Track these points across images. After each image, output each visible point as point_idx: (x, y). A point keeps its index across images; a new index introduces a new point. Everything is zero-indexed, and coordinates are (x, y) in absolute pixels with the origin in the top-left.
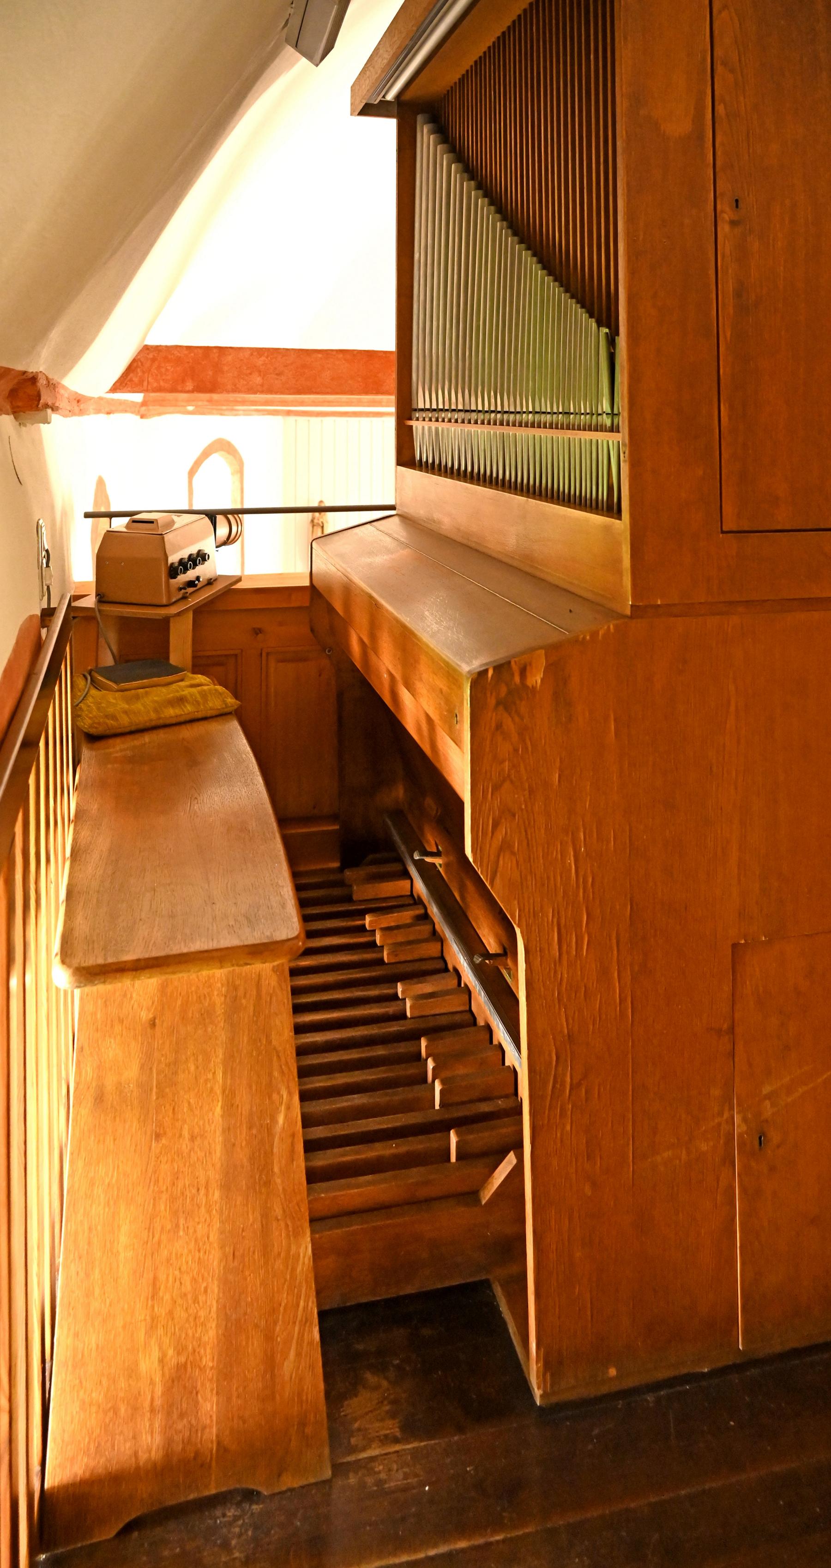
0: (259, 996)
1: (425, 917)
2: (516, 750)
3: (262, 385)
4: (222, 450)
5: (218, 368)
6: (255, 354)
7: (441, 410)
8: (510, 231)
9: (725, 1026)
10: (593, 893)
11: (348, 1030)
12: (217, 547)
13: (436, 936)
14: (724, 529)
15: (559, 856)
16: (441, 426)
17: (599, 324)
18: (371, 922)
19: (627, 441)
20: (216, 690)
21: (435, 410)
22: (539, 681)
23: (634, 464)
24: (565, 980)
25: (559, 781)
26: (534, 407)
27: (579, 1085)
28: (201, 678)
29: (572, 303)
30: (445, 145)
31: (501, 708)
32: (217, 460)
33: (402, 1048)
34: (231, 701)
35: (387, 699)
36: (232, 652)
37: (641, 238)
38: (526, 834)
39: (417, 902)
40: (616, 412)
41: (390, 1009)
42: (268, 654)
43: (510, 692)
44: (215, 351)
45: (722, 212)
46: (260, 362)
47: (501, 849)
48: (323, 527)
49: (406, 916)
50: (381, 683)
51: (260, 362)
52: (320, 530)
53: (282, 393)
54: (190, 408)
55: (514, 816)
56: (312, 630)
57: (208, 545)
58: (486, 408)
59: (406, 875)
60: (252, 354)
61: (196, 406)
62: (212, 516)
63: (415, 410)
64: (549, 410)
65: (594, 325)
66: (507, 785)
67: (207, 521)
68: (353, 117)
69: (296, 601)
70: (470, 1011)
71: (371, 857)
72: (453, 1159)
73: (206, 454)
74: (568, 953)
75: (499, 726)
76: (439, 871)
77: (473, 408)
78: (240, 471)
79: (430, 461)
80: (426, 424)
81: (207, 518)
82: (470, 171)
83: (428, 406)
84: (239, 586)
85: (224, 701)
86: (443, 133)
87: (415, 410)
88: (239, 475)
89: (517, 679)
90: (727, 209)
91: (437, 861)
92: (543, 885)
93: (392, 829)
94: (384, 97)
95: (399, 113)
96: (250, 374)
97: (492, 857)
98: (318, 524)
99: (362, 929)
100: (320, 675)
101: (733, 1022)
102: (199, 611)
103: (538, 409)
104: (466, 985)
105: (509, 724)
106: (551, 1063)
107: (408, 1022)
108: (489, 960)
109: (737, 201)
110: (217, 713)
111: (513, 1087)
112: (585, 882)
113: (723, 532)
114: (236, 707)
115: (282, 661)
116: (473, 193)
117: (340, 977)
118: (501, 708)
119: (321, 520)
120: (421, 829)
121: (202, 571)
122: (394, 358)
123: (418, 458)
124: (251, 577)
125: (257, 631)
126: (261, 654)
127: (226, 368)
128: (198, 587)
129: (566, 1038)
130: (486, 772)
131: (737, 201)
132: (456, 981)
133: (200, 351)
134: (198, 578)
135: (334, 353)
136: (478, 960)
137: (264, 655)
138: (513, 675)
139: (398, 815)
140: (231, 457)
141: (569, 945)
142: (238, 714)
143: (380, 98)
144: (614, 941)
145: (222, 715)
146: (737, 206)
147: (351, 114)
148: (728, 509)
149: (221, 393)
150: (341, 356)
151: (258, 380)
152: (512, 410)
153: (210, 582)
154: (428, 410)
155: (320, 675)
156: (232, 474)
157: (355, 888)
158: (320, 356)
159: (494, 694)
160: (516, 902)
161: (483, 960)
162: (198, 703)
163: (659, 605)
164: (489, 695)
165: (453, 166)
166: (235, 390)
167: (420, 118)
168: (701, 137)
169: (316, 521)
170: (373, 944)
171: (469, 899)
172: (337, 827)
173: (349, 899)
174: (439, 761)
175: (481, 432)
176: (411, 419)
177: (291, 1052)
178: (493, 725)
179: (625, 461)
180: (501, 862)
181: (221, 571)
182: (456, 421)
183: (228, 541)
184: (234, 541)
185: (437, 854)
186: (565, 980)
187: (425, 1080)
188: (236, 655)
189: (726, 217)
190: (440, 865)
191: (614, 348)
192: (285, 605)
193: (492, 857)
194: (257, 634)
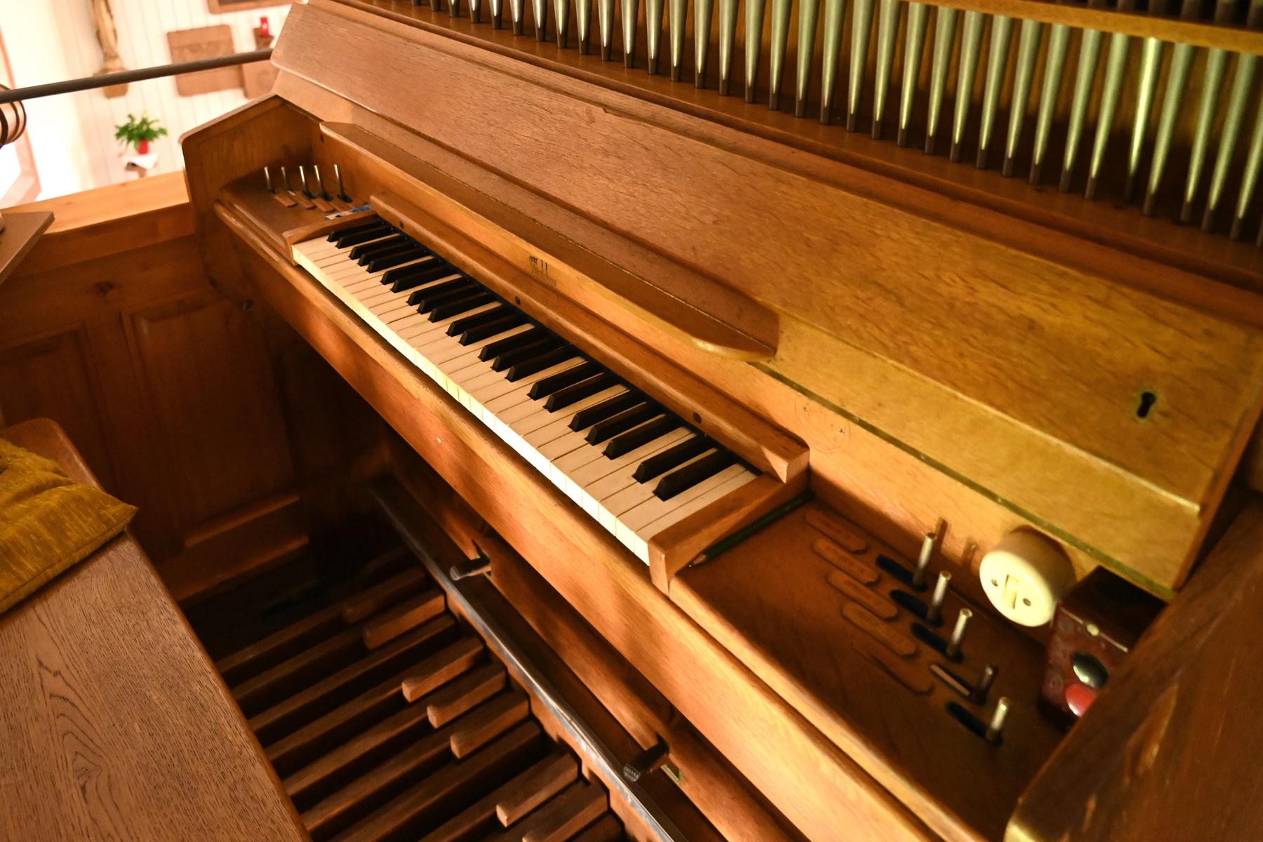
1: (486, 659)
34: (119, 511)
39: (462, 629)
69: (165, 233)
85: (100, 517)
91: (485, 570)
104: (591, 773)
136: (635, 777)
157: (368, 634)
162: (48, 547)
173: (359, 651)
185: (483, 562)
190: (489, 573)
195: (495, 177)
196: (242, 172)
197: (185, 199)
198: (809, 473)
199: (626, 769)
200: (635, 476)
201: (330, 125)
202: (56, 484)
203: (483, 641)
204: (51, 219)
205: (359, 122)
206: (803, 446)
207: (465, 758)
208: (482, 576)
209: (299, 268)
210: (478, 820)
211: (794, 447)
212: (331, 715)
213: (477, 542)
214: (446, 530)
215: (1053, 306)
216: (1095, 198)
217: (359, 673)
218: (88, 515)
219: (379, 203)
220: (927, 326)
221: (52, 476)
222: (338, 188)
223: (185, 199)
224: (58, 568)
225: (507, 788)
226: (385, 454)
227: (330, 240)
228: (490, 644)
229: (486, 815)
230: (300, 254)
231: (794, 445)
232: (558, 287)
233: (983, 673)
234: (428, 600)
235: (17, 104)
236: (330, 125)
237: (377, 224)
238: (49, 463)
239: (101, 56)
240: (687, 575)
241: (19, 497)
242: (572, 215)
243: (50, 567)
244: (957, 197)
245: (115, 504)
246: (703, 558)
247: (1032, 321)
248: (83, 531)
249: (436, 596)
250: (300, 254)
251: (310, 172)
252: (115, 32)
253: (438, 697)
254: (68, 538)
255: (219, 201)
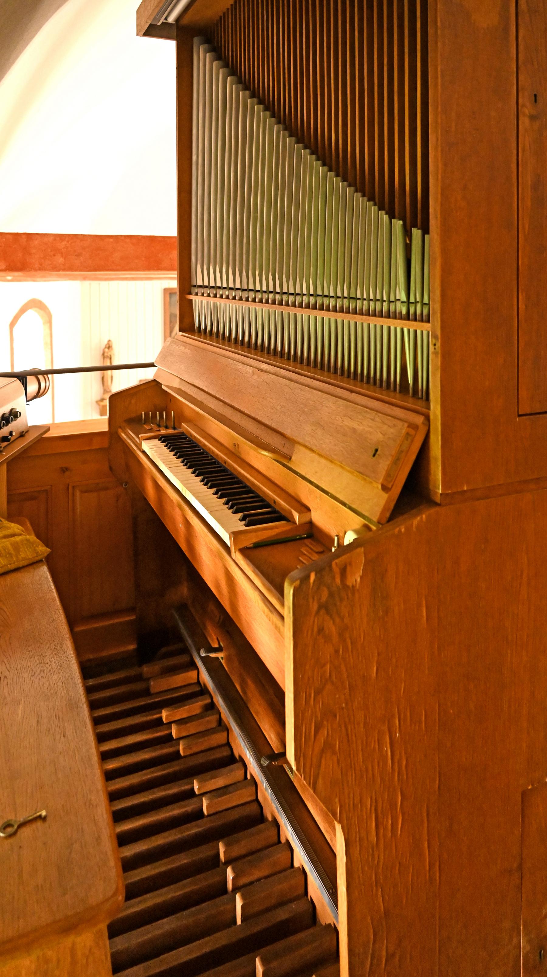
0: (74, 962)
1: (211, 707)
2: (337, 651)
3: (64, 265)
4: (35, 307)
5: (26, 250)
6: (58, 239)
7: (219, 288)
8: (287, 133)
9: (515, 865)
10: (407, 774)
11: (153, 838)
12: (27, 401)
13: (222, 726)
14: (520, 413)
15: (377, 747)
16: (218, 301)
17: (392, 216)
18: (167, 717)
19: (439, 333)
20: (28, 540)
21: (213, 287)
22: (359, 580)
23: (446, 356)
24: (382, 861)
25: (377, 673)
26: (315, 290)
27: (393, 955)
28: (15, 527)
29: (358, 195)
30: (220, 62)
31: (323, 611)
32: (32, 314)
33: (202, 853)
34: (43, 550)
35: (183, 546)
36: (43, 488)
37: (453, 128)
38: (347, 730)
39: (204, 691)
40: (412, 300)
41: (188, 807)
42: (73, 487)
43: (331, 595)
44: (23, 236)
45: (524, 106)
46: (62, 245)
47: (323, 751)
48: (111, 359)
49: (195, 707)
50: (177, 530)
51: (62, 245)
52: (108, 361)
53: (81, 271)
54: (9, 278)
55: (336, 716)
56: (111, 468)
57: (19, 403)
58: (264, 289)
59: (193, 665)
60: (55, 240)
61: (14, 276)
62: (22, 377)
63: (195, 286)
64: (332, 294)
65: (386, 218)
66: (329, 686)
67: (18, 383)
68: (139, 37)
69: (96, 444)
70: (257, 800)
71: (164, 650)
72: (239, 922)
73: (23, 310)
74: (385, 835)
75: (321, 630)
76: (220, 662)
77: (251, 287)
78: (49, 321)
79: (209, 328)
80: (205, 300)
81: (18, 381)
82: (244, 83)
83: (206, 283)
84: (47, 435)
85: (35, 550)
86: (218, 52)
87: (195, 286)
88: (48, 325)
89: (338, 581)
90: (528, 104)
91: (220, 655)
92: (362, 777)
93: (180, 624)
94: (166, 19)
95: (177, 36)
96: (54, 255)
97: (315, 760)
98: (107, 357)
99: (159, 722)
100: (117, 500)
101: (522, 859)
102: (11, 463)
103: (319, 292)
104: (252, 776)
105: (332, 628)
106: (369, 942)
107: (205, 820)
108: (274, 762)
109: (535, 95)
110: (30, 562)
111: (304, 887)
112: (400, 762)
113: (519, 416)
114: (46, 555)
115: (86, 492)
116: (249, 100)
117: (145, 778)
118: (323, 611)
119: (109, 353)
120: (205, 627)
121: (15, 426)
122: (177, 244)
123: (197, 325)
124: (59, 425)
125: (64, 470)
126: (68, 488)
127: (33, 251)
128: (11, 440)
129: (383, 915)
130: (309, 679)
131: (535, 95)
132: (242, 772)
133: (11, 237)
134: (11, 433)
135: (123, 238)
136: (265, 763)
137: (70, 489)
138: (334, 578)
139: (182, 608)
140: (42, 312)
141: (385, 829)
142: (49, 560)
143: (162, 20)
144: (425, 814)
145: (34, 564)
146: (536, 101)
147: (138, 35)
148: (523, 393)
149: (30, 271)
150: (128, 240)
151: (61, 260)
152: (292, 291)
153: (22, 435)
154: (207, 287)
155: (117, 500)
156: (44, 324)
157: (152, 683)
158: (111, 240)
159: (316, 598)
160: (337, 800)
161: (270, 763)
162: (10, 554)
163: (465, 491)
164: (311, 600)
165: (229, 79)
166: (42, 268)
167: (196, 40)
168: (506, 30)
169: (106, 354)
170: (169, 738)
171: (249, 695)
172: (133, 617)
173: (146, 692)
174: (240, 620)
175: (260, 310)
176: (190, 293)
177: (95, 759)
178: (316, 629)
179: (435, 353)
180: (323, 761)
181: (31, 423)
182: (234, 298)
183: (38, 395)
184: (44, 393)
185: (219, 650)
186: (382, 861)
187: (224, 890)
188: (46, 491)
189: (526, 111)
190: (222, 658)
191: (411, 240)
192: (87, 448)
193: (315, 760)
194: (64, 472)
195: (221, 403)
196: (133, 415)
197: (106, 429)
198: (311, 523)
199: (263, 759)
200: (239, 520)
201: (168, 387)
202: (21, 535)
203: (212, 698)
204: (48, 430)
205: (181, 387)
206: (309, 510)
207: (185, 757)
208: (217, 658)
209: (144, 452)
210: (183, 788)
211: (303, 509)
212: (120, 721)
213: (219, 639)
214: (206, 634)
215: (361, 423)
216: (400, 392)
217: (143, 703)
218: (30, 548)
219: (186, 427)
220: (329, 436)
221: (20, 531)
222: (172, 423)
223: (107, 430)
224: (13, 566)
225: (202, 776)
226: (184, 590)
227: (159, 440)
228: (215, 700)
229: (216, 879)
230: (146, 446)
231: (305, 509)
232: (243, 456)
233: (529, 785)
234: (188, 671)
235: (45, 376)
236: (165, 385)
237: (183, 436)
238: (20, 527)
239: (102, 391)
240: (244, 551)
241: (6, 537)
242: (242, 415)
243: (10, 564)
244: (352, 391)
245: (42, 546)
246: (252, 545)
247: (355, 429)
248: (26, 555)
249: (193, 670)
250: (146, 446)
251: (161, 416)
252: (112, 377)
253: (180, 722)
254: (20, 555)
255: (120, 427)
